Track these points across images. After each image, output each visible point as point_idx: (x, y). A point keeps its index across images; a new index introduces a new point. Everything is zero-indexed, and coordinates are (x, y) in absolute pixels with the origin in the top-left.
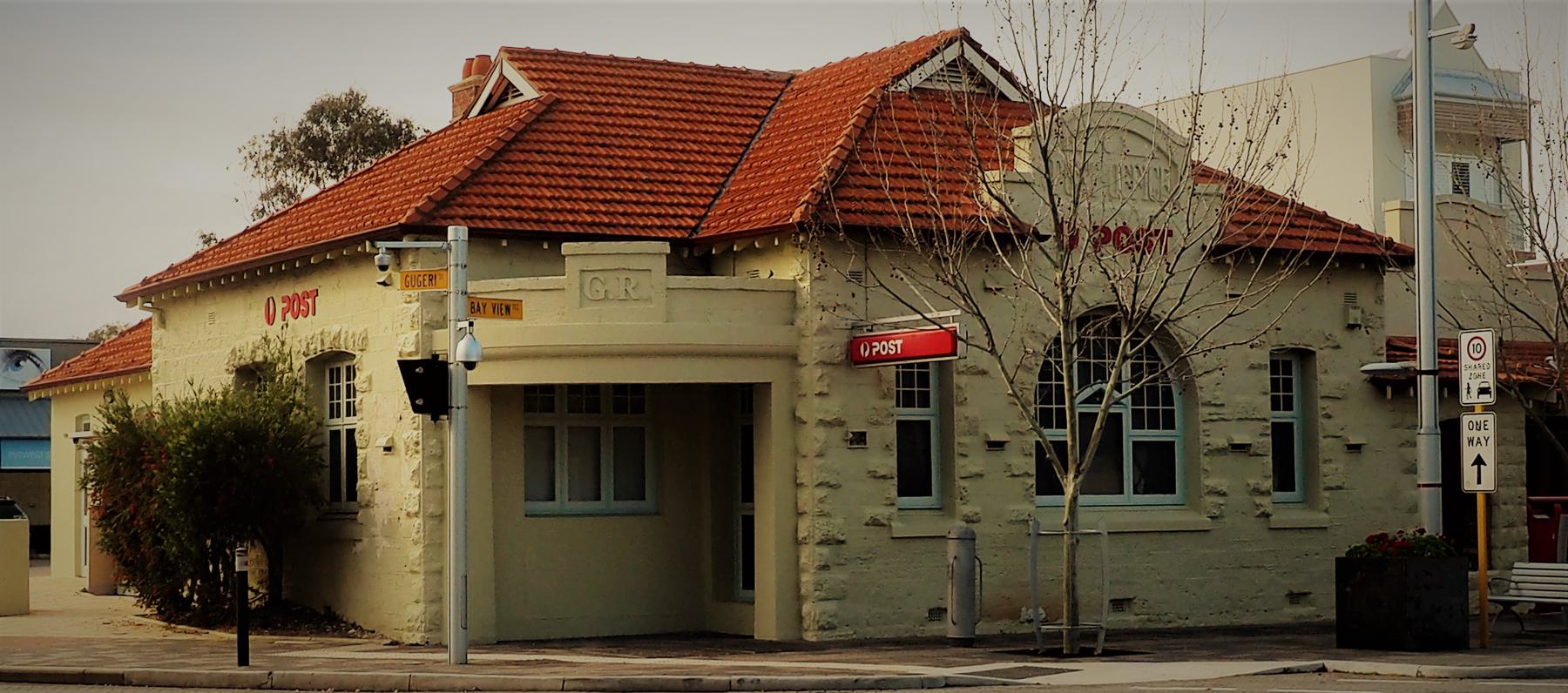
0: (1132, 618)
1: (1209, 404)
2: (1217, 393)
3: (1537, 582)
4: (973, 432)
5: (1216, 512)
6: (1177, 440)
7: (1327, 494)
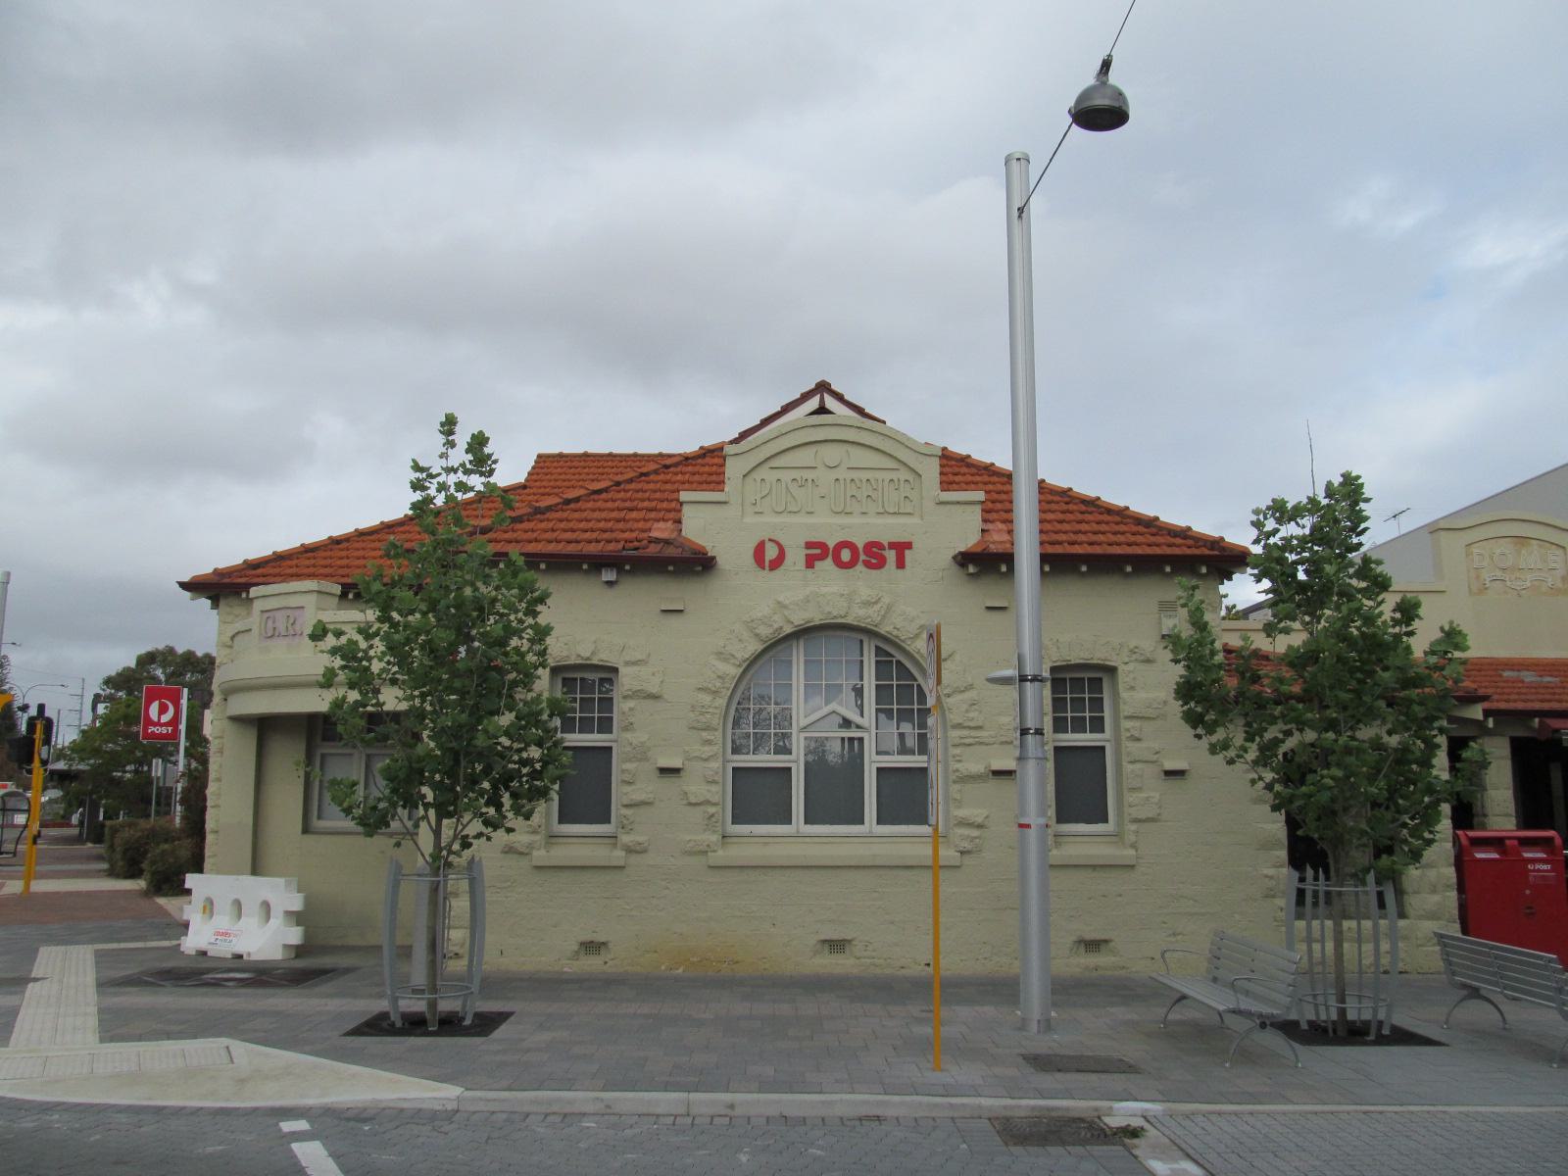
0: (852, 961)
1: (959, 726)
2: (971, 715)
3: (34, 850)
4: (1015, 746)
5: (967, 845)
6: (794, 766)
7: (1133, 827)
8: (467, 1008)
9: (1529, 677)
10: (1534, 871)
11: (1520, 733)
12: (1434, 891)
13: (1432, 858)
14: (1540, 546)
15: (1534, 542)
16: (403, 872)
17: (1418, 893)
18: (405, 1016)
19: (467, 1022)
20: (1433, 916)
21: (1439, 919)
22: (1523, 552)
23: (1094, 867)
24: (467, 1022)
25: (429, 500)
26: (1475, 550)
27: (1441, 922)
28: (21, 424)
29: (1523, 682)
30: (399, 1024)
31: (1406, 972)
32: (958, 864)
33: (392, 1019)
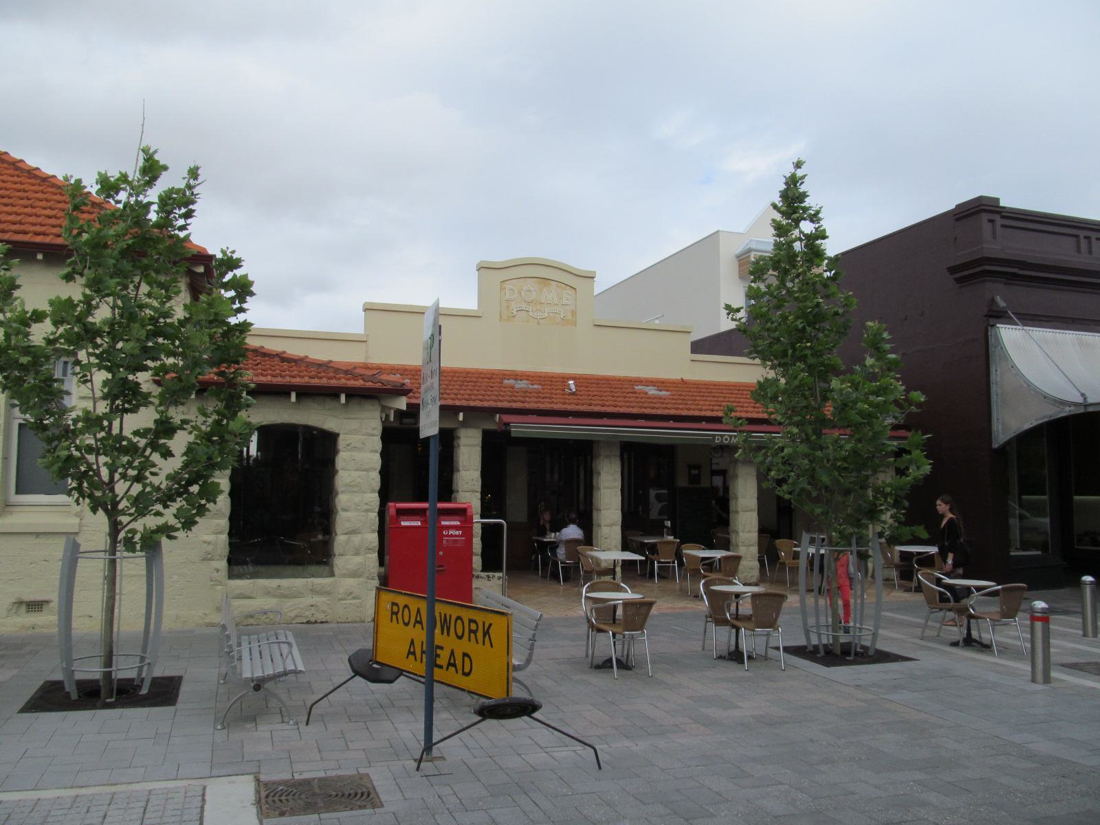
8: (144, 675)
9: (652, 391)
10: (448, 536)
11: (491, 426)
12: (357, 554)
13: (358, 525)
14: (556, 285)
15: (554, 283)
16: (82, 549)
17: (342, 555)
18: (80, 684)
19: (144, 691)
20: (354, 574)
21: (359, 576)
22: (544, 290)
23: (37, 534)
24: (144, 691)
25: (790, 244)
26: (508, 286)
27: (360, 579)
28: (71, 103)
29: (646, 393)
30: (74, 696)
31: (327, 622)
32: (77, 531)
33: (67, 689)
